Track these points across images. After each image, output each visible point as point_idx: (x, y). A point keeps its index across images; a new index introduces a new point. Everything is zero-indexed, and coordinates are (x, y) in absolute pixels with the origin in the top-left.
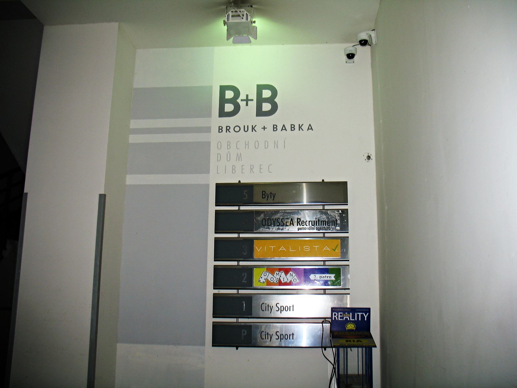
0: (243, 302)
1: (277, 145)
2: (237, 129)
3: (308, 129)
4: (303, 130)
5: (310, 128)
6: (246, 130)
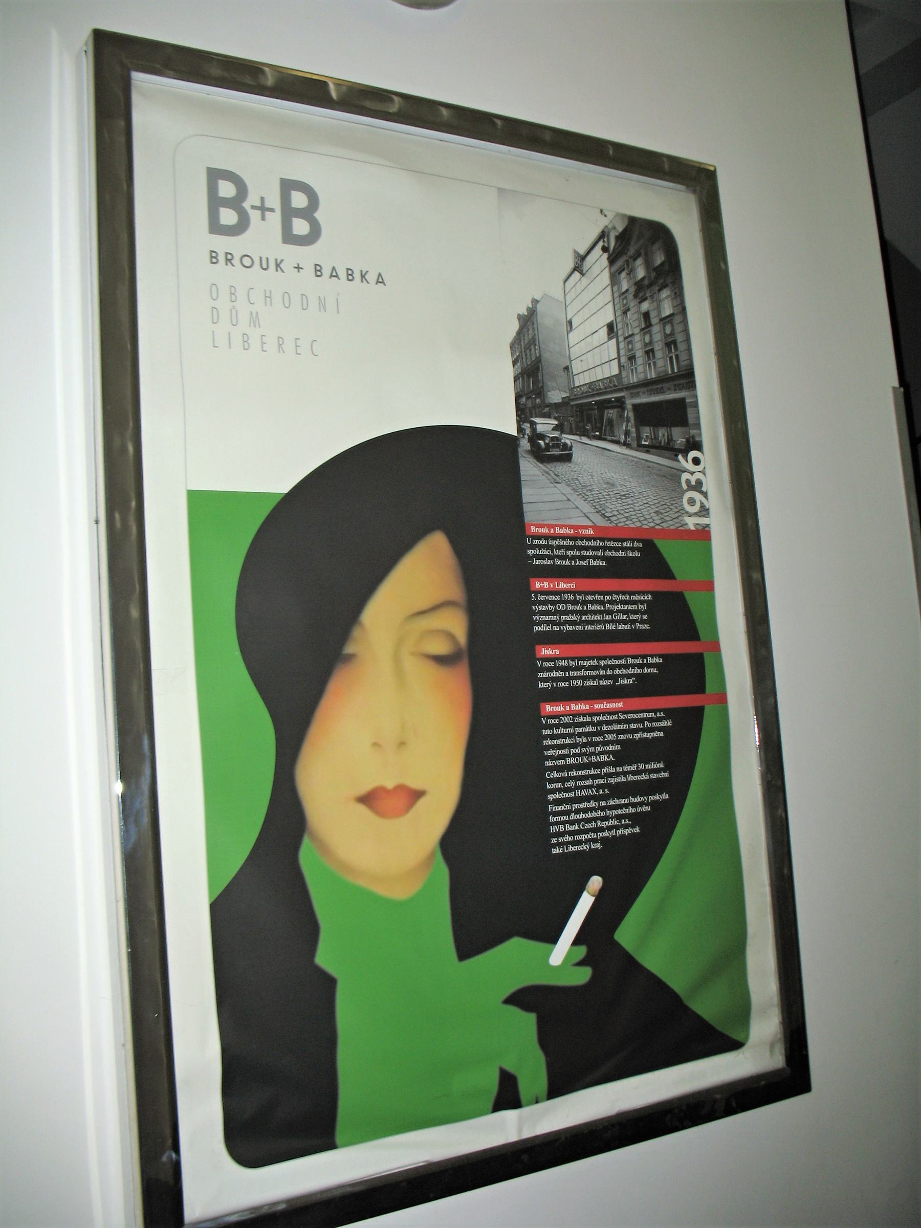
1: (325, 304)
4: (368, 282)
5: (380, 280)
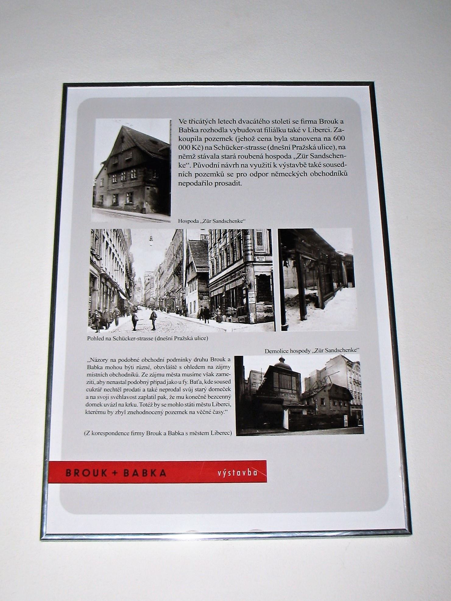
0: (318, 410)
2: (86, 473)
3: (161, 475)
6: (96, 474)
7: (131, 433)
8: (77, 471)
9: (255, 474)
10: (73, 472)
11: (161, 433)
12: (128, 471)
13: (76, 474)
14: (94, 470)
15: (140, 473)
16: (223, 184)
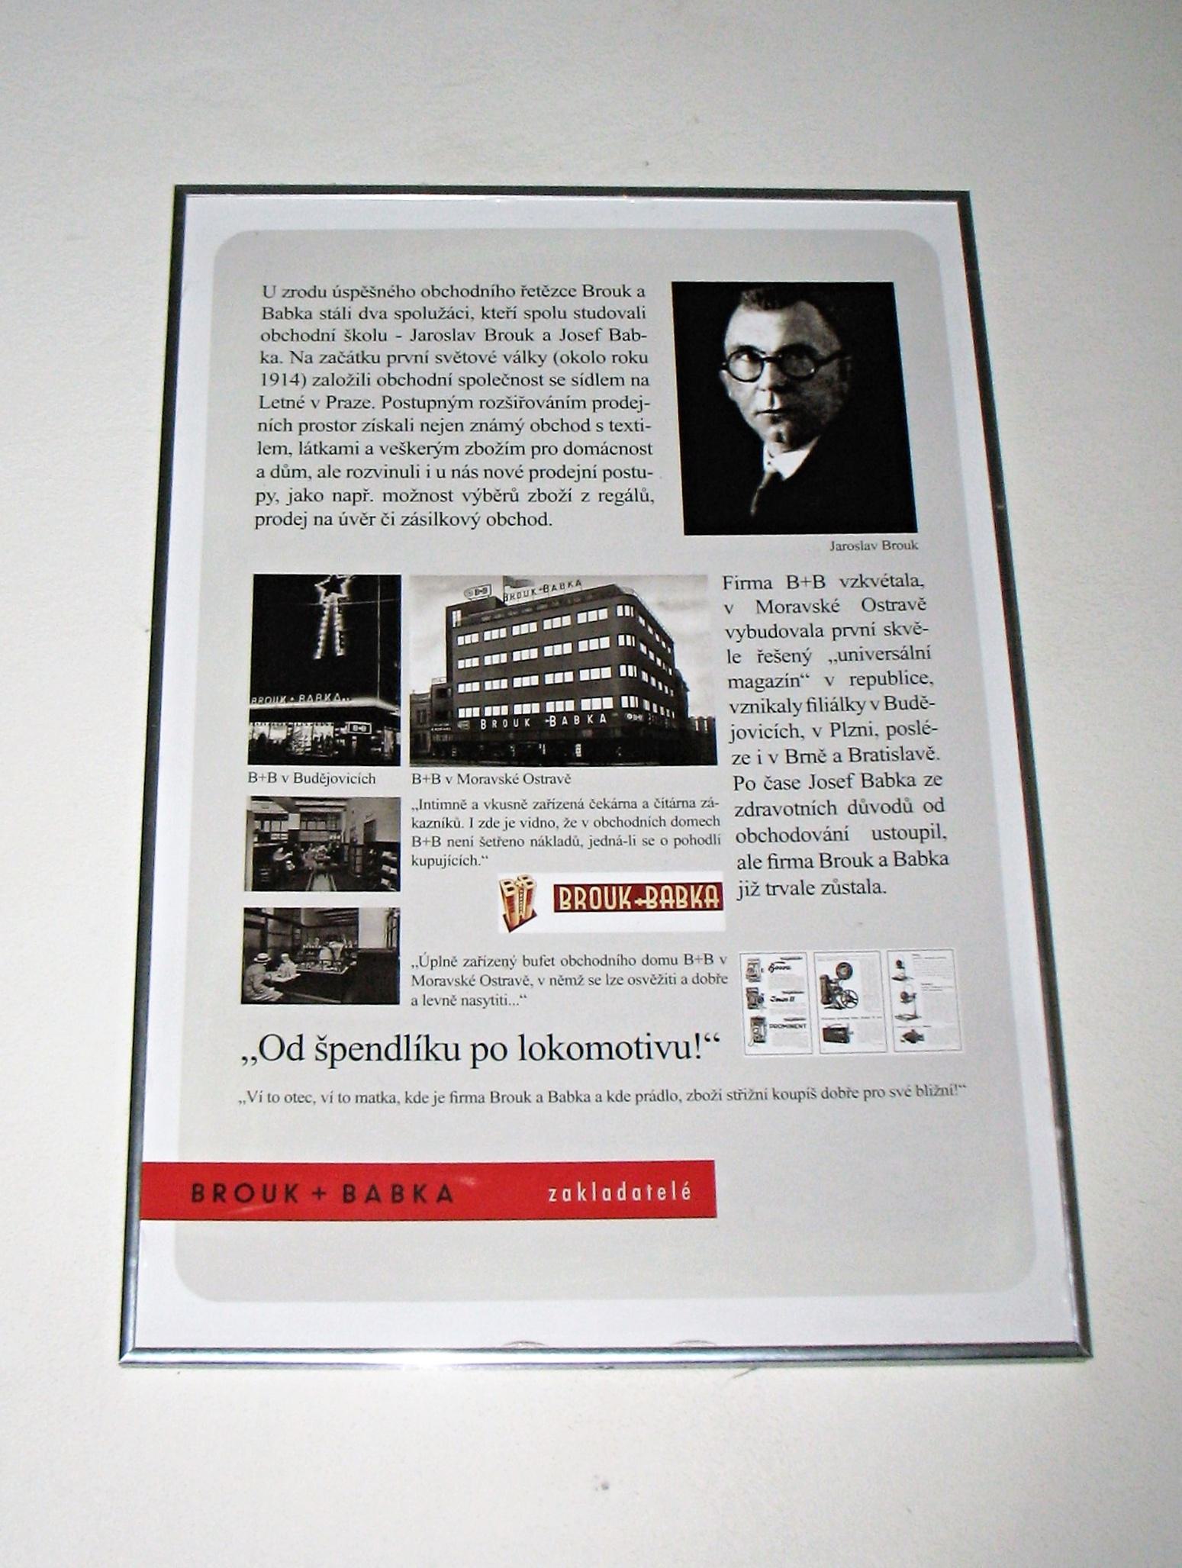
3: (440, 1198)
7: (450, 1098)
8: (220, 1189)
9: (606, 1196)
10: (209, 1193)
11: (529, 1095)
12: (402, 1190)
13: (218, 1196)
14: (265, 1186)
15: (385, 1193)
16: (320, 427)
